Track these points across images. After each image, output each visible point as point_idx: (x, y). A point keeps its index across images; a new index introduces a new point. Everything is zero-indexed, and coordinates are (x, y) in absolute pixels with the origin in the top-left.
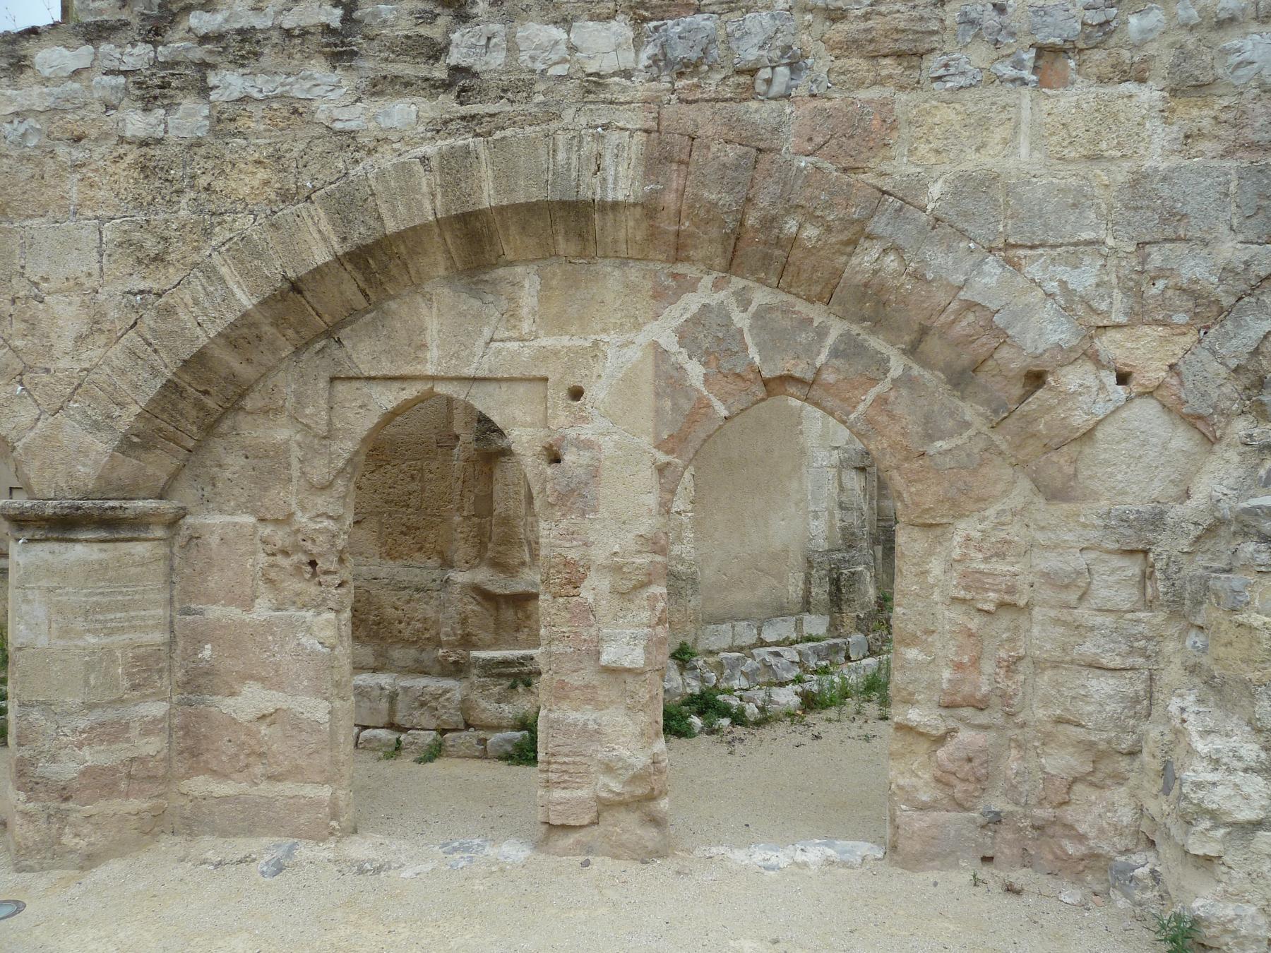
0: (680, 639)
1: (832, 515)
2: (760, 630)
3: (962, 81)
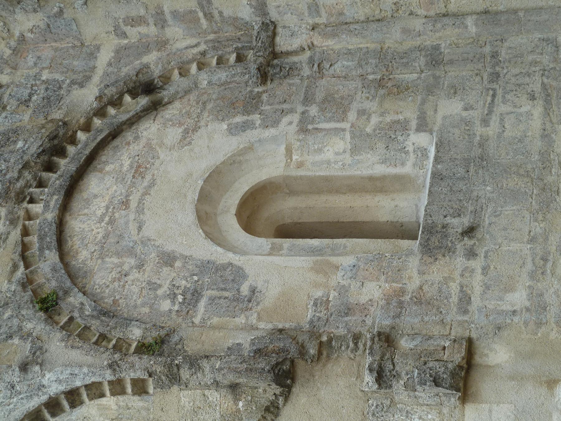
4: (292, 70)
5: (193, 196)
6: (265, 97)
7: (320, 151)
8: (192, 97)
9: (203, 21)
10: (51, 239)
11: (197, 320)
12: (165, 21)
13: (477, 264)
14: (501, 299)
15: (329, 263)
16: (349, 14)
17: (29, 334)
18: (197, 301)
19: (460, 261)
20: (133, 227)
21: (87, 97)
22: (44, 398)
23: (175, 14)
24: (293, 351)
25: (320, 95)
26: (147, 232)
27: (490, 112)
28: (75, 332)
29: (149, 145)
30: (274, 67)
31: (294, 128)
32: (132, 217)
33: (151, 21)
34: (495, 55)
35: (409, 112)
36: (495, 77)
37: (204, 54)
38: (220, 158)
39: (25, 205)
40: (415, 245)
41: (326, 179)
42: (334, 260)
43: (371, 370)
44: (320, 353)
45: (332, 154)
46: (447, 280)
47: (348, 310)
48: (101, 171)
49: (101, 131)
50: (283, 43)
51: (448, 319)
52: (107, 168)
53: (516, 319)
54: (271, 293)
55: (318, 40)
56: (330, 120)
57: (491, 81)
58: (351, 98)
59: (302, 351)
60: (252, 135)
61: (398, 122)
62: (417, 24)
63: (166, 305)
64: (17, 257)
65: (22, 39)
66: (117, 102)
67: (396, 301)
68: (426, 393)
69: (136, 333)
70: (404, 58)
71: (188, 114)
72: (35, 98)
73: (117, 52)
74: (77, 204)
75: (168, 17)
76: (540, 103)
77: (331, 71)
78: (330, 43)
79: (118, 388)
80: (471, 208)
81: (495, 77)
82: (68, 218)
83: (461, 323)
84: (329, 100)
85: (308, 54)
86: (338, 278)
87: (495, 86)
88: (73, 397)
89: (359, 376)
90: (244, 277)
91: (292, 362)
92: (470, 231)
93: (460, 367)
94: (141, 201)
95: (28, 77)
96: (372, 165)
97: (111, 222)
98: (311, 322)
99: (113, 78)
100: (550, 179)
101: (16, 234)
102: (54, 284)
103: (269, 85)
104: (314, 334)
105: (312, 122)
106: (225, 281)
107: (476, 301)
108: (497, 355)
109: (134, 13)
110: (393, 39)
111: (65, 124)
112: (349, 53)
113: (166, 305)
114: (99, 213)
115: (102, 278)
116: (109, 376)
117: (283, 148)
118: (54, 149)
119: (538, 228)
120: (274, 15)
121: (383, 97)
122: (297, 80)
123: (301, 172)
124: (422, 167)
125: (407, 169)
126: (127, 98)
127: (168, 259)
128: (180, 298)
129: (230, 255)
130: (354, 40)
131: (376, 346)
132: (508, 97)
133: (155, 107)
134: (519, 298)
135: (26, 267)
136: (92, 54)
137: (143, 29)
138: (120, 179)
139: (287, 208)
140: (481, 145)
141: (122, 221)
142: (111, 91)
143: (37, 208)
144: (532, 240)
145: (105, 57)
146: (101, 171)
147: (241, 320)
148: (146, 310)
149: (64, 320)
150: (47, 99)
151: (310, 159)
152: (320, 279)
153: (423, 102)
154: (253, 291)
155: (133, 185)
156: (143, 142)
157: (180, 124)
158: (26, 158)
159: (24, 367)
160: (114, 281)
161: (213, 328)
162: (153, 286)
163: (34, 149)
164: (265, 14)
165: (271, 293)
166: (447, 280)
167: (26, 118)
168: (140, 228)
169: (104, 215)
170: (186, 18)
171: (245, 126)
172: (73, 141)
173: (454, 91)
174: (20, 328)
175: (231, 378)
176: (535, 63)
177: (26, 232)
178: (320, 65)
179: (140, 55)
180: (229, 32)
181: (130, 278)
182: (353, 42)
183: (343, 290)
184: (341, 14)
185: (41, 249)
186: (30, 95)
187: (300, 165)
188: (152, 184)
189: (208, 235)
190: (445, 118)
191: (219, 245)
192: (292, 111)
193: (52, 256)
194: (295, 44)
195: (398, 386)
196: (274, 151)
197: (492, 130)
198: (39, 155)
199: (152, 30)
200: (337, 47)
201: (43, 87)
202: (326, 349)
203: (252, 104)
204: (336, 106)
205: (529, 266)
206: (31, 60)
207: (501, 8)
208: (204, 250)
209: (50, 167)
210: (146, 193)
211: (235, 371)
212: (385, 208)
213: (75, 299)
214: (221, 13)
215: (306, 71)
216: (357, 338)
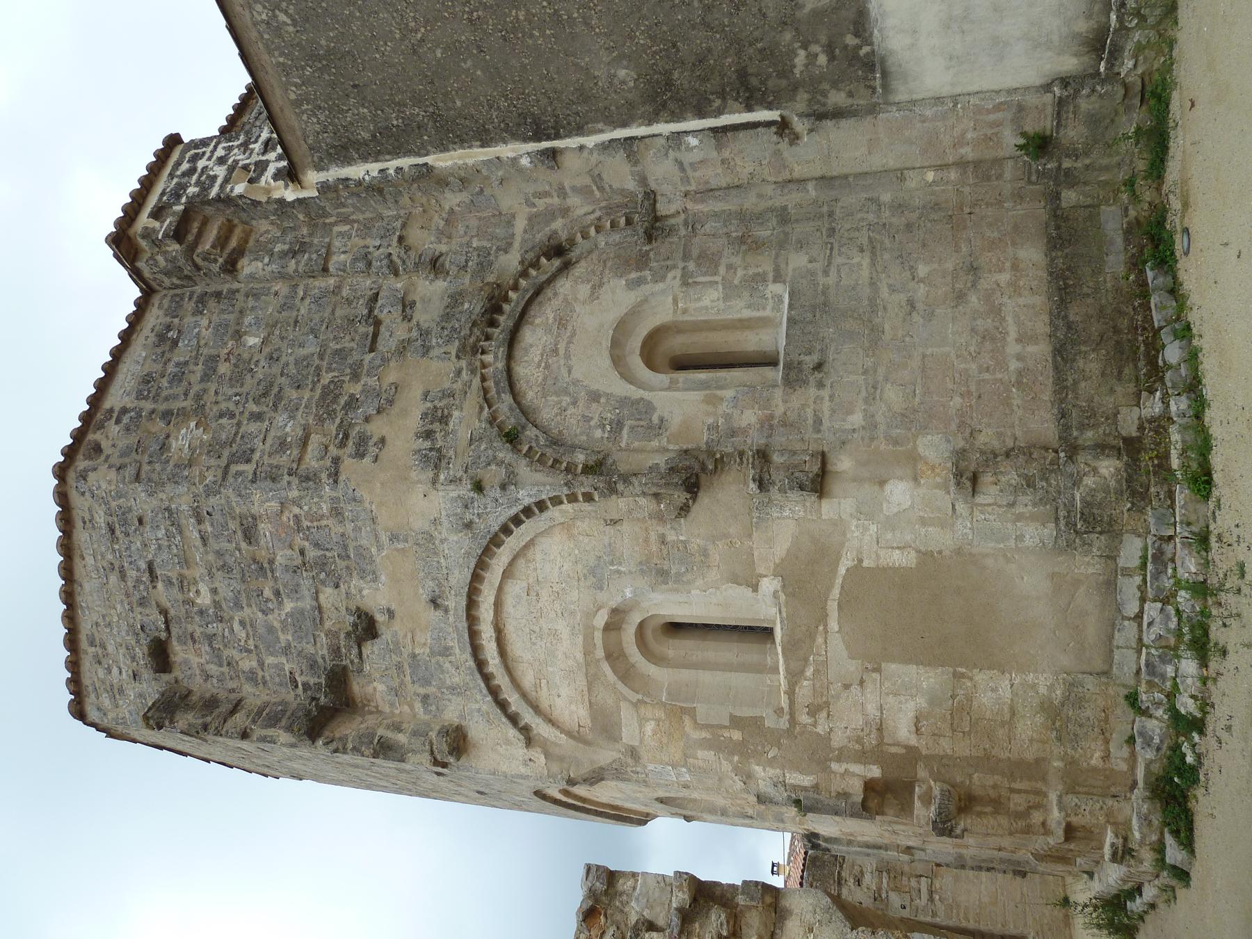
0: (1122, 700)
1: (1019, 517)
2: (1124, 618)
3: (409, 636)
4: (672, 230)
5: (606, 343)
6: (652, 255)
7: (699, 299)
8: (594, 256)
9: (597, 193)
10: (504, 384)
11: (623, 445)
12: (566, 193)
13: (825, 393)
14: (844, 420)
15: (715, 396)
16: (714, 184)
17: (503, 462)
18: (621, 429)
19: (812, 391)
20: (564, 371)
21: (511, 261)
22: (521, 507)
23: (574, 189)
24: (697, 467)
25: (695, 252)
26: (576, 374)
27: (829, 264)
28: (537, 460)
29: (565, 300)
30: (657, 229)
31: (677, 282)
32: (562, 362)
33: (555, 194)
34: (831, 214)
35: (765, 264)
36: (832, 232)
37: (599, 219)
38: (622, 311)
39: (479, 356)
40: (777, 374)
41: (706, 322)
42: (719, 393)
43: (754, 480)
44: (716, 467)
45: (708, 302)
46: (804, 406)
47: (733, 433)
48: (532, 324)
49: (527, 291)
50: (663, 208)
51: (806, 438)
52: (538, 321)
53: (855, 435)
54: (675, 422)
55: (690, 205)
56: (705, 274)
57: (829, 236)
58: (720, 253)
59: (704, 468)
60: (647, 289)
61: (758, 274)
62: (769, 190)
63: (598, 433)
64: (481, 400)
65: (452, 211)
66: (535, 264)
67: (767, 424)
68: (794, 495)
69: (580, 458)
70: (760, 217)
71: (593, 271)
72: (470, 263)
73: (530, 219)
74: (518, 353)
75: (568, 191)
76: (867, 254)
77: (703, 231)
78: (700, 207)
79: (572, 498)
80: (819, 347)
81: (832, 232)
82: (513, 364)
83: (816, 440)
84: (702, 256)
85: (683, 216)
86: (724, 408)
87: (832, 240)
88: (541, 506)
89: (745, 483)
90: (654, 409)
91: (697, 475)
92: (819, 367)
93: (817, 475)
94: (567, 349)
95: (461, 245)
96: (740, 309)
97: (547, 367)
98: (707, 443)
99: (530, 244)
100: (877, 320)
101: (477, 381)
102: (513, 420)
103: (654, 244)
104: (710, 453)
105: (692, 276)
106: (640, 413)
107: (826, 423)
108: (843, 464)
109: (540, 189)
110: (750, 202)
111: (498, 285)
112: (716, 215)
113: (598, 433)
114: (536, 360)
115: (547, 414)
116: (566, 491)
117: (670, 299)
118: (494, 307)
119: (869, 363)
120: (653, 186)
121: (745, 252)
122: (676, 239)
123: (687, 318)
124: (779, 310)
125: (768, 313)
126: (543, 260)
127: (595, 397)
128: (608, 428)
129: (642, 392)
130: (720, 204)
131: (757, 462)
132: (843, 250)
133: (566, 266)
134: (857, 419)
135: (490, 407)
136: (509, 222)
137: (548, 200)
138: (548, 331)
139: (678, 344)
140: (824, 293)
141: (555, 366)
142: (530, 256)
143: (488, 358)
144: (865, 372)
145: (520, 224)
146: (532, 324)
147: (655, 443)
148: (584, 438)
149: (525, 448)
150: (480, 264)
151: (693, 305)
152: (710, 409)
153: (777, 256)
154: (662, 420)
155: (559, 335)
156: (561, 298)
157: (589, 281)
158: (473, 317)
159: (503, 487)
160: (556, 415)
161: (635, 450)
162: (587, 419)
163: (478, 309)
164: (646, 185)
165: (675, 422)
166: (804, 406)
167: (467, 281)
168: (570, 372)
169: (540, 361)
170: (584, 191)
171: (640, 282)
172: (506, 299)
173: (801, 245)
174: (495, 458)
175: (654, 490)
176: (863, 219)
177: (483, 379)
178: (693, 224)
179: (548, 223)
180: (618, 199)
181: (569, 412)
182: (718, 206)
183: (728, 417)
184: (707, 183)
185: (498, 393)
186: (467, 261)
187: (685, 311)
188: (573, 334)
189: (623, 376)
190: (794, 270)
191: (631, 383)
192: (675, 267)
193: (507, 398)
194: (672, 209)
195: (774, 491)
196: (663, 302)
197: (831, 280)
198: (483, 314)
199: (556, 201)
200: (706, 209)
201: (475, 253)
202: (720, 463)
203: (642, 262)
204: (709, 261)
205: (864, 394)
206: (461, 229)
207: (835, 174)
208: (621, 388)
209: (493, 323)
210: (569, 342)
211: (657, 485)
212: (752, 342)
213: (531, 432)
214: (610, 186)
215: (683, 232)
216: (741, 454)
